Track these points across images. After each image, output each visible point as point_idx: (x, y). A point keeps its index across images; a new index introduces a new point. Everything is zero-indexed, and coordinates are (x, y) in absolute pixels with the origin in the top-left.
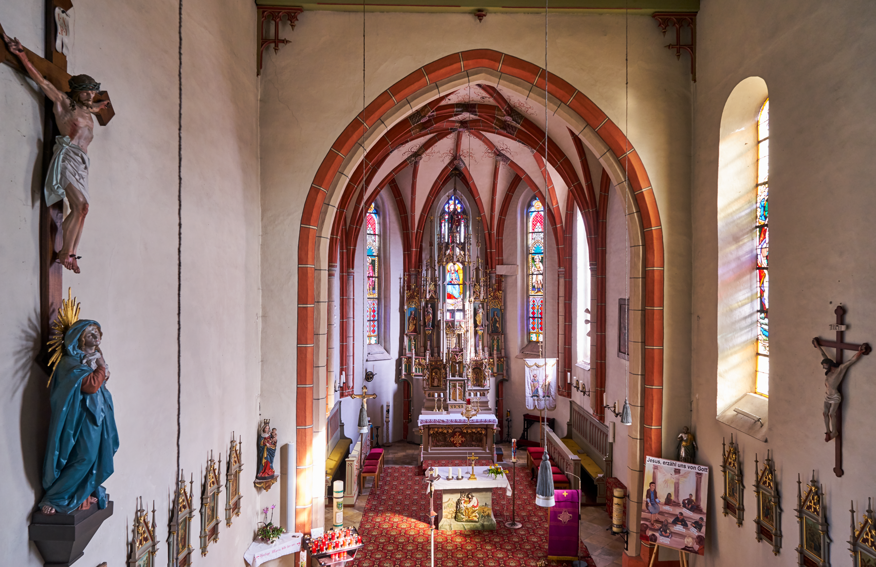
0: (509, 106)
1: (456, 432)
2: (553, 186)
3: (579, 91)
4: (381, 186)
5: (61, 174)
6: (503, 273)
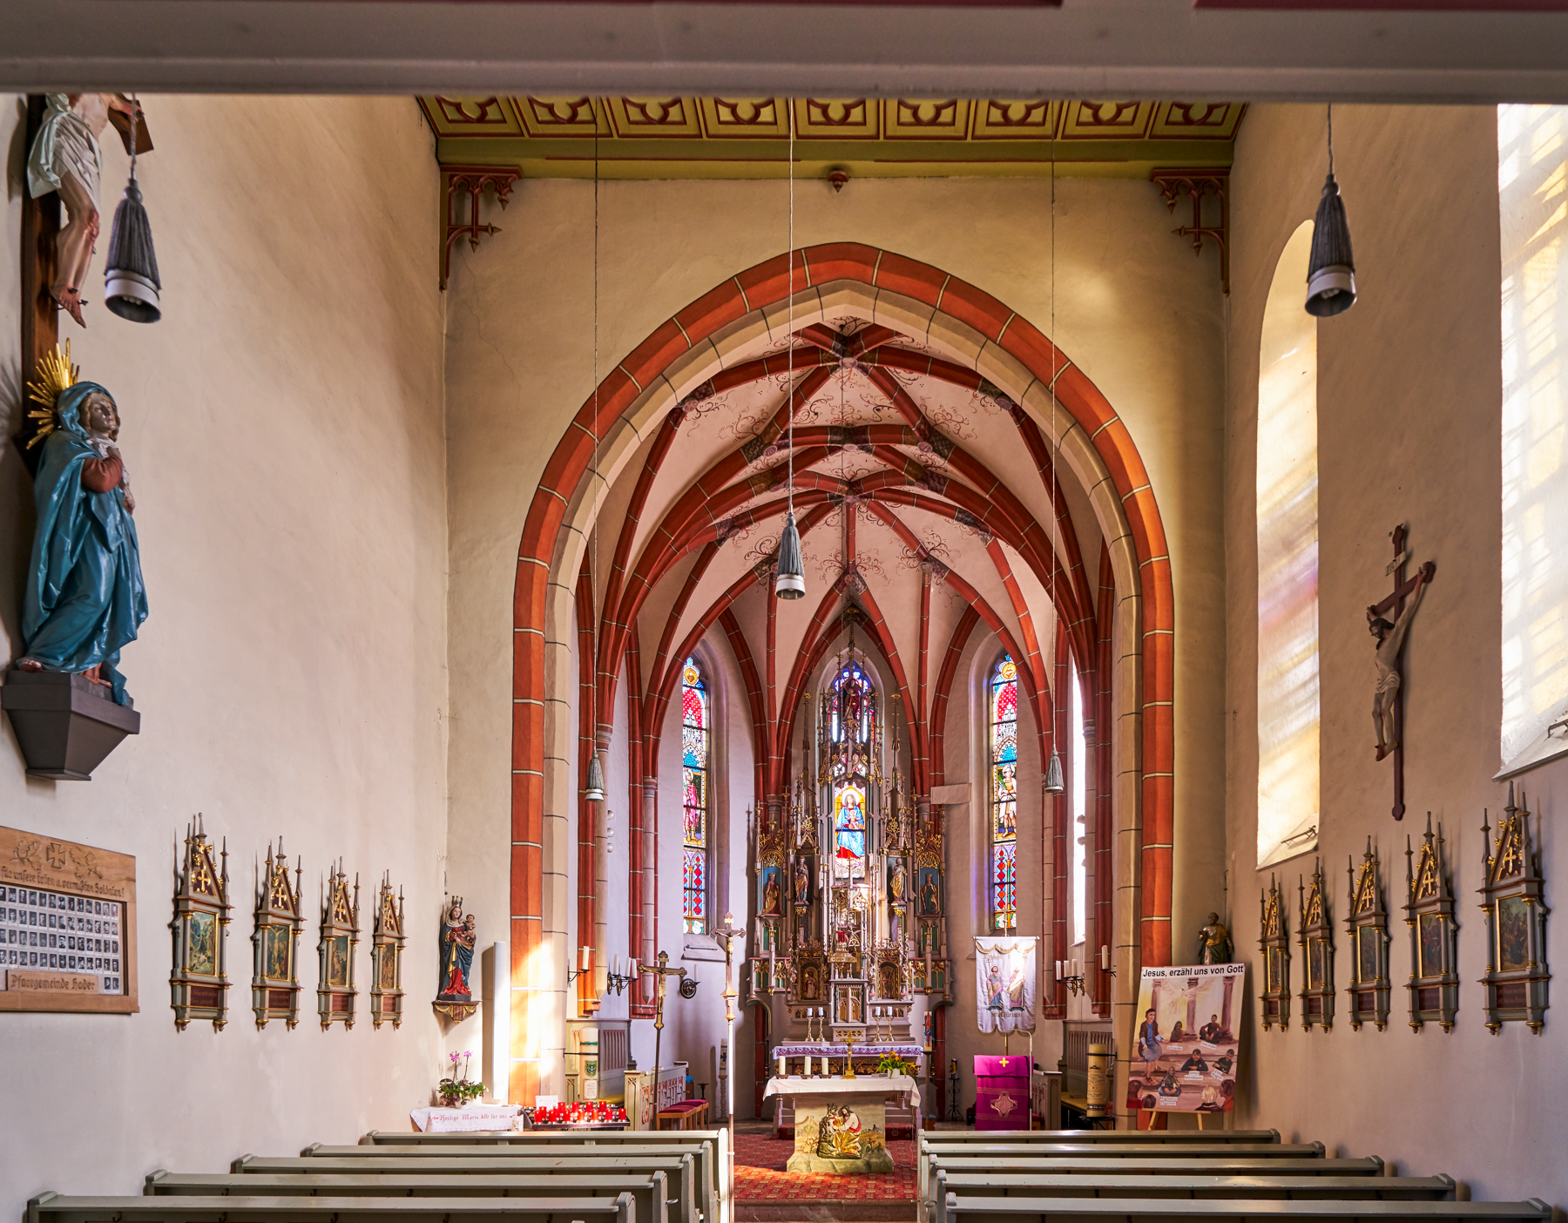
0: (925, 421)
2: (1028, 614)
3: (1016, 314)
4: (705, 620)
5: (54, 154)
6: (944, 801)
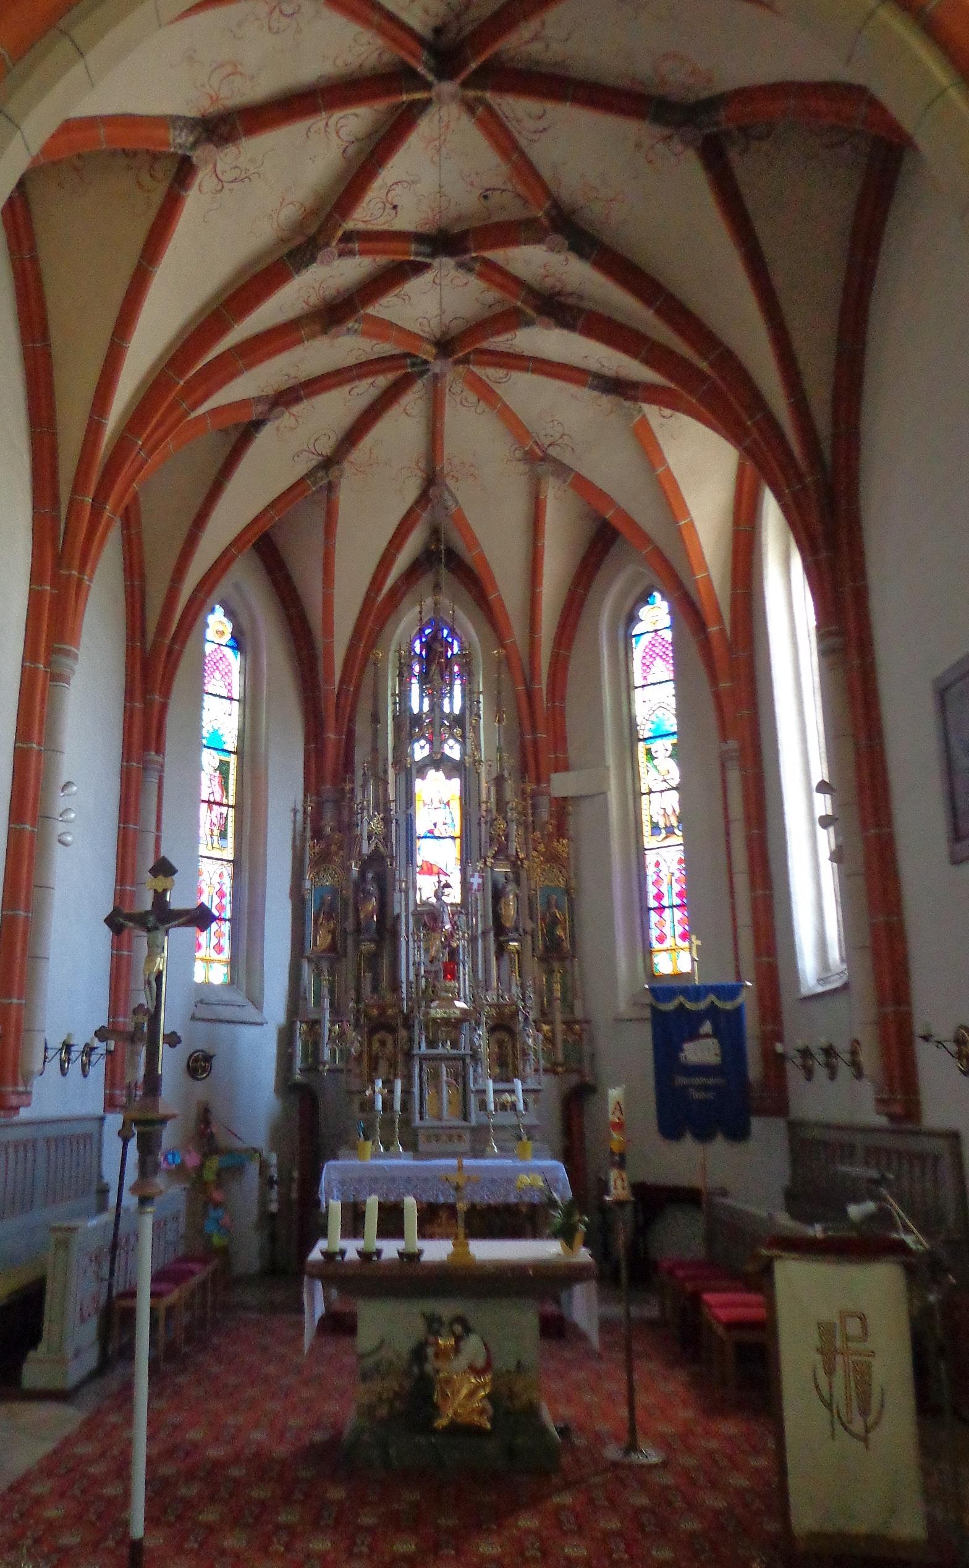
0: (556, 204)
6: (570, 793)
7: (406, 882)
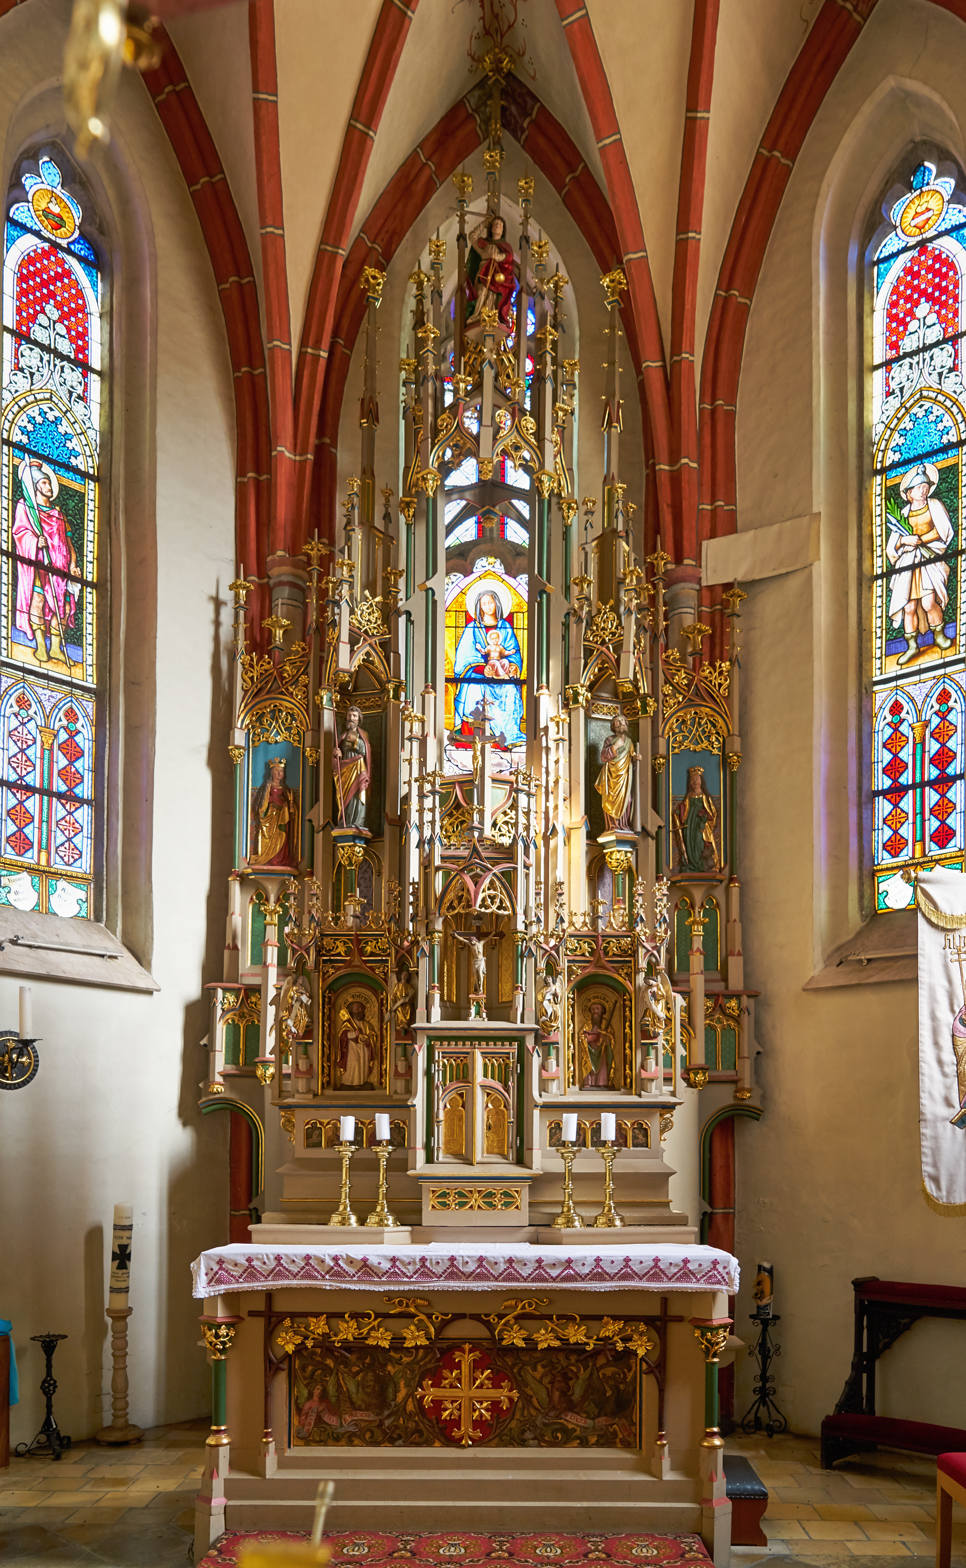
1: (457, 1345)
6: (739, 573)
7: (423, 722)
